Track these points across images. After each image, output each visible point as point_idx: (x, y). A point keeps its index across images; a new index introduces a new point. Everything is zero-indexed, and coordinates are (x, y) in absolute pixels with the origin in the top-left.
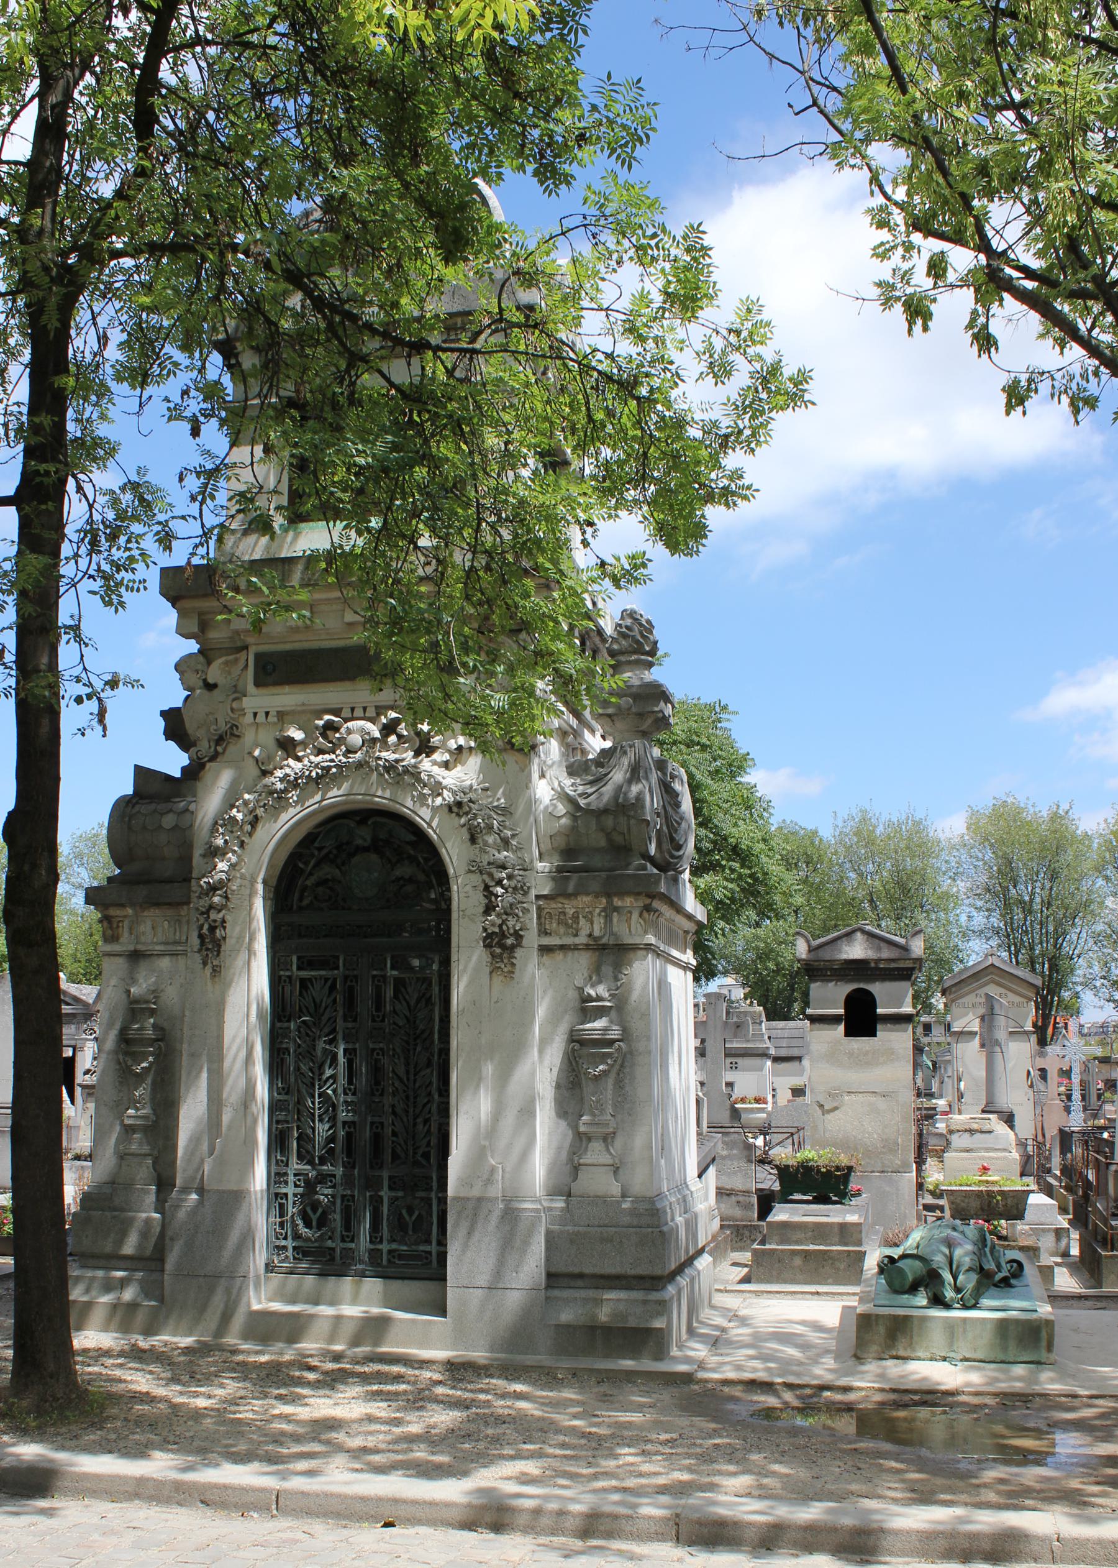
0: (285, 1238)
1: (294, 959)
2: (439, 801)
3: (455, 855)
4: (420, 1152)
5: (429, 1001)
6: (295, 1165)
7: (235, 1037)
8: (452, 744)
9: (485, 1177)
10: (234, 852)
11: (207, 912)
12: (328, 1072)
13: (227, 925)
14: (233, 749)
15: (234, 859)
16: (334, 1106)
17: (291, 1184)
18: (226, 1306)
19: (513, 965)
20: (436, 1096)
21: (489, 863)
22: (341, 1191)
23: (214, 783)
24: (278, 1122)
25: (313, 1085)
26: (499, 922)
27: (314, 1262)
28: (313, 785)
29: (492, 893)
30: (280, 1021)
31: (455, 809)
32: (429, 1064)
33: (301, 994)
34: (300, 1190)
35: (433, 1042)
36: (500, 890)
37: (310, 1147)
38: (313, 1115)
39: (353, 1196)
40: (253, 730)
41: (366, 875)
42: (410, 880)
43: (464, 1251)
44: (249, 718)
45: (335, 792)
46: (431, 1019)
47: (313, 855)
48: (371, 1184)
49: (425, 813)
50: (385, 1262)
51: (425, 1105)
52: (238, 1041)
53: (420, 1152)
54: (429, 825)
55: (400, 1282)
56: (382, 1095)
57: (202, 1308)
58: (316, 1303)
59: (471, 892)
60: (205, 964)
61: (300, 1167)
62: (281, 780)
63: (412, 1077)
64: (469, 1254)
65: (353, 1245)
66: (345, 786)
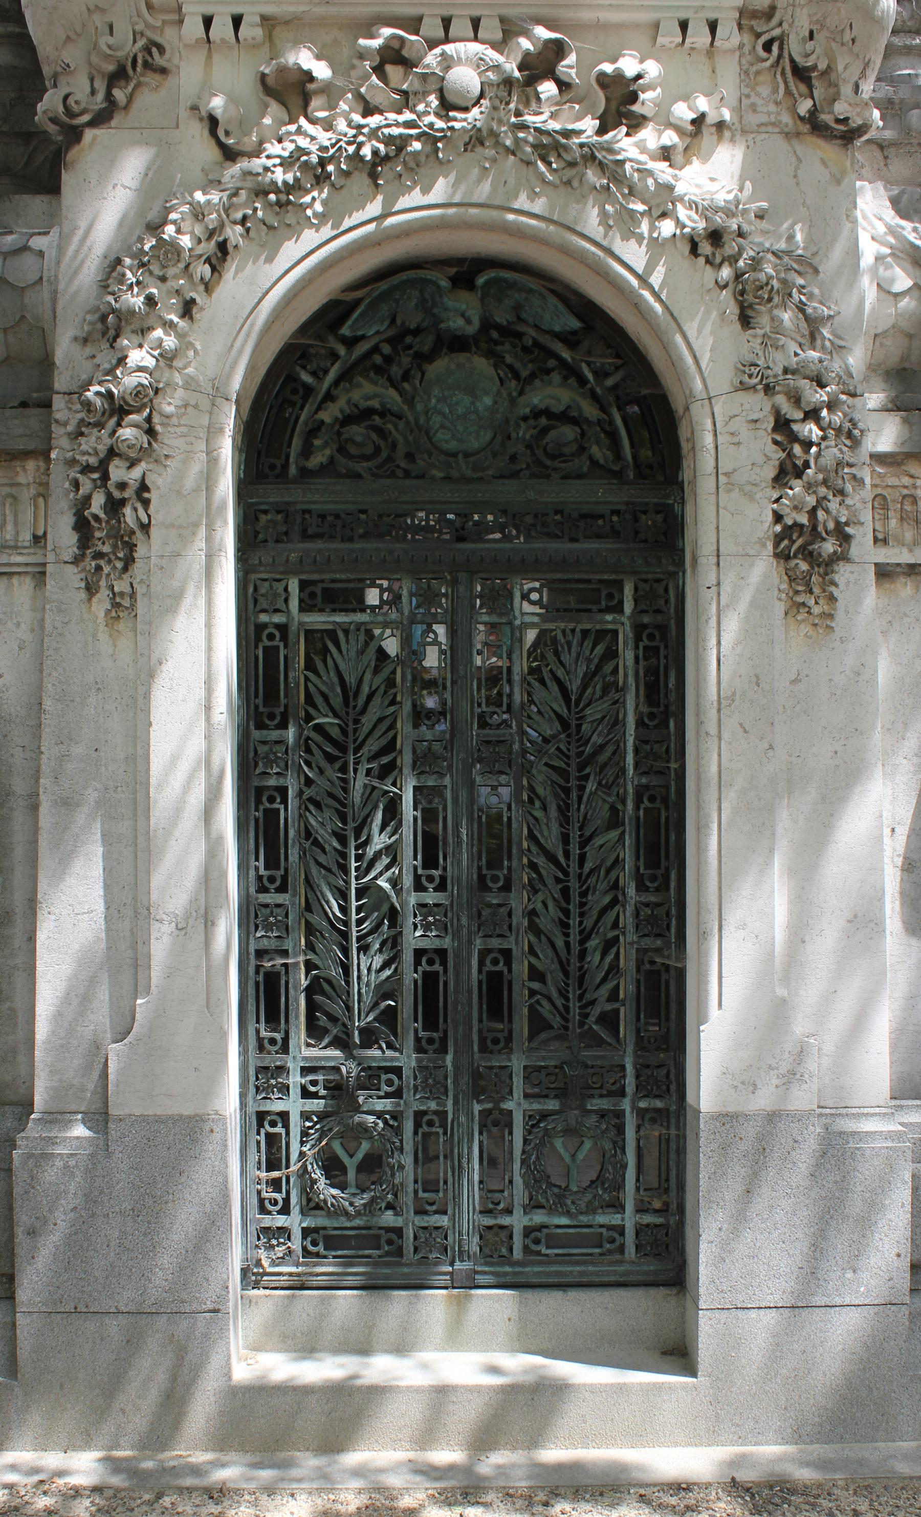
0: (285, 1210)
1: (294, 586)
2: (667, 228)
3: (702, 350)
4: (596, 1011)
5: (612, 687)
6: (304, 1050)
7: (174, 759)
8: (683, 112)
9: (784, 1067)
10: (169, 326)
11: (103, 468)
12: (379, 841)
13: (153, 496)
14: (149, 100)
15: (170, 342)
16: (393, 915)
17: (295, 1092)
18: (174, 1379)
19: (832, 599)
20: (631, 891)
21: (786, 371)
22: (413, 1103)
23: (105, 176)
24: (260, 954)
25: (345, 869)
26: (811, 500)
27: (348, 1261)
28: (361, 181)
29: (794, 438)
30: (260, 726)
31: (706, 248)
32: (615, 820)
33: (310, 665)
34: (317, 1105)
35: (623, 770)
36: (812, 431)
37: (337, 1008)
38: (345, 935)
39: (442, 1114)
40: (200, 56)
41: (464, 401)
42: (565, 417)
43: (736, 1231)
44: (193, 28)
45: (415, 198)
46: (617, 723)
47: (334, 356)
48: (486, 1085)
49: (635, 254)
50: (518, 1254)
51: (603, 912)
52: (184, 767)
53: (596, 1011)
54: (643, 280)
55: (558, 1295)
56: (507, 887)
57: (111, 1385)
58: (364, 1350)
59: (745, 433)
60: (91, 589)
61: (314, 1052)
62: (286, 163)
63: (575, 850)
64: (748, 1236)
65: (444, 1221)
66: (440, 190)
